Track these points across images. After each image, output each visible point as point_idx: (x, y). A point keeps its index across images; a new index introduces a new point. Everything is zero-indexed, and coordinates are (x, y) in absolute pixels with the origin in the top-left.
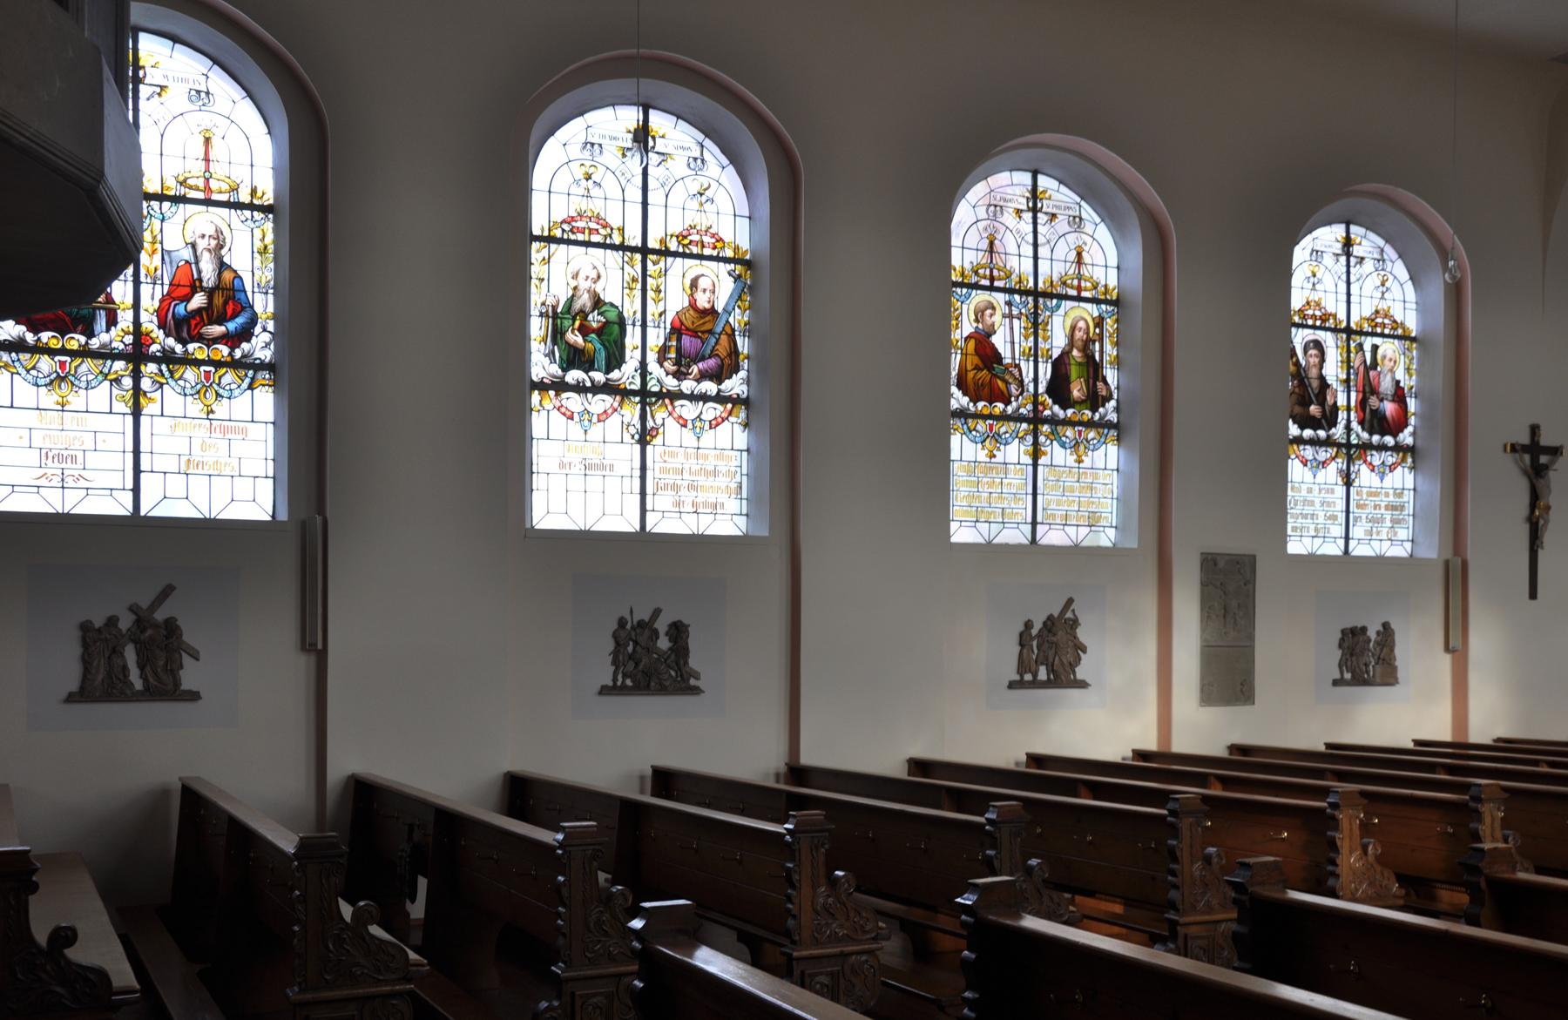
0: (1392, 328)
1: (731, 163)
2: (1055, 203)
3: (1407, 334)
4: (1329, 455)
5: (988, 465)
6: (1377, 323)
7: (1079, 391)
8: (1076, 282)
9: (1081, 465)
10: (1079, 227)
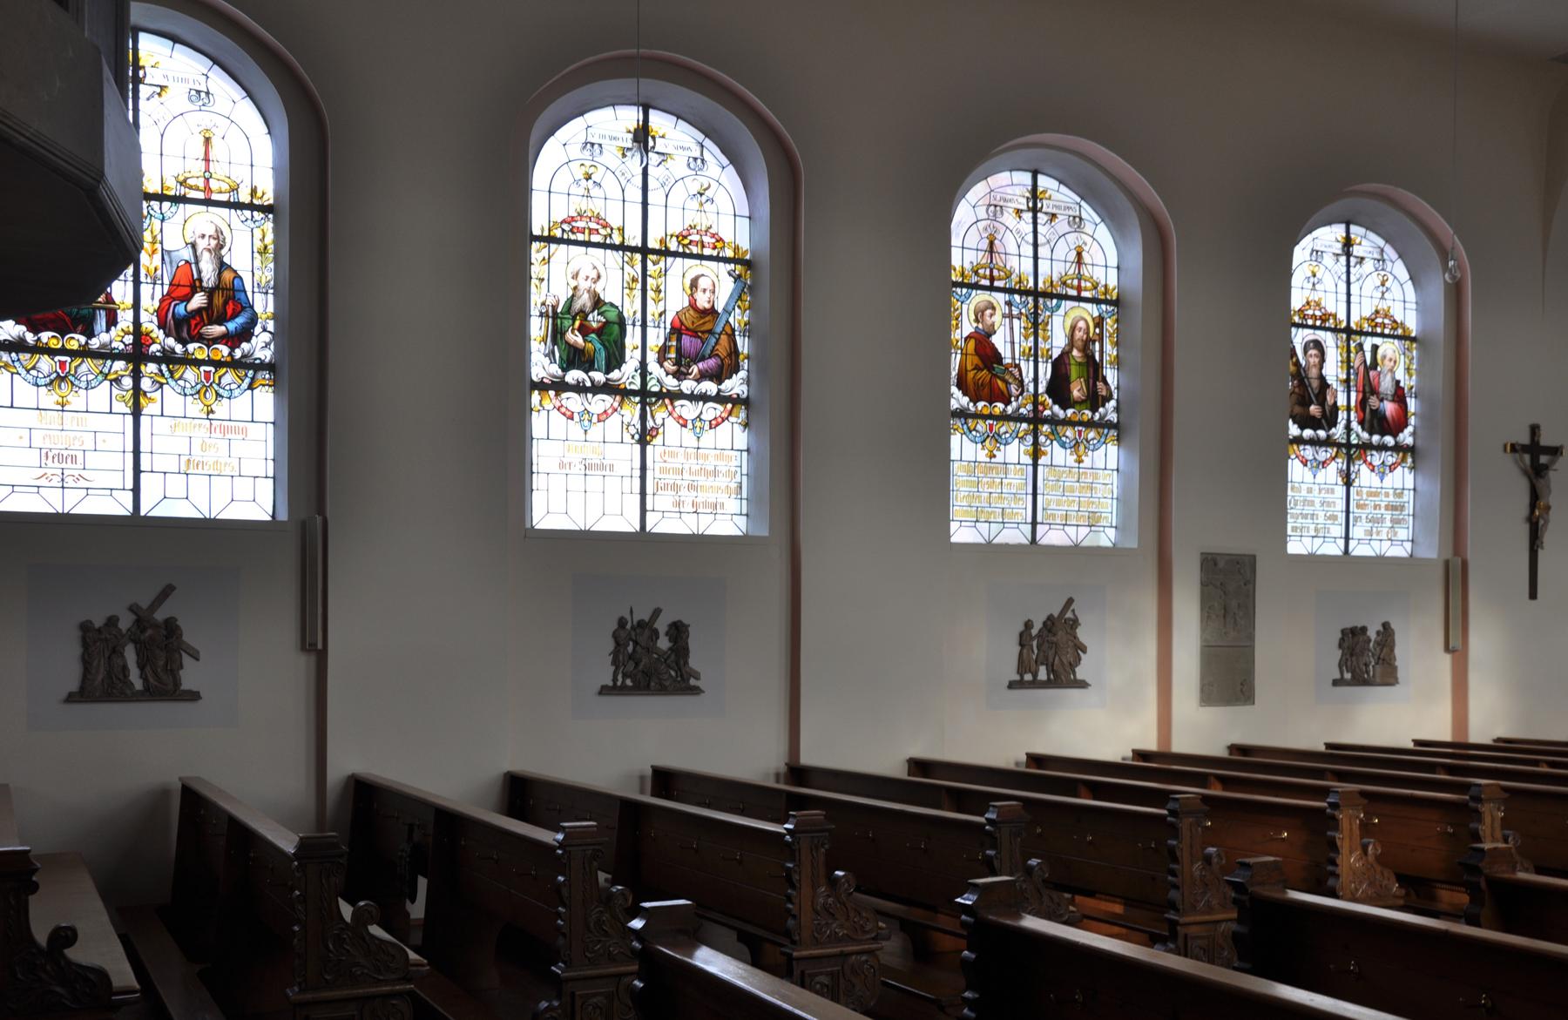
0: (1392, 328)
2: (1055, 203)
3: (1407, 334)
4: (1329, 455)
5: (988, 465)
6: (1377, 323)
7: (1079, 391)
8: (1076, 282)
9: (1081, 465)
10: (1079, 227)
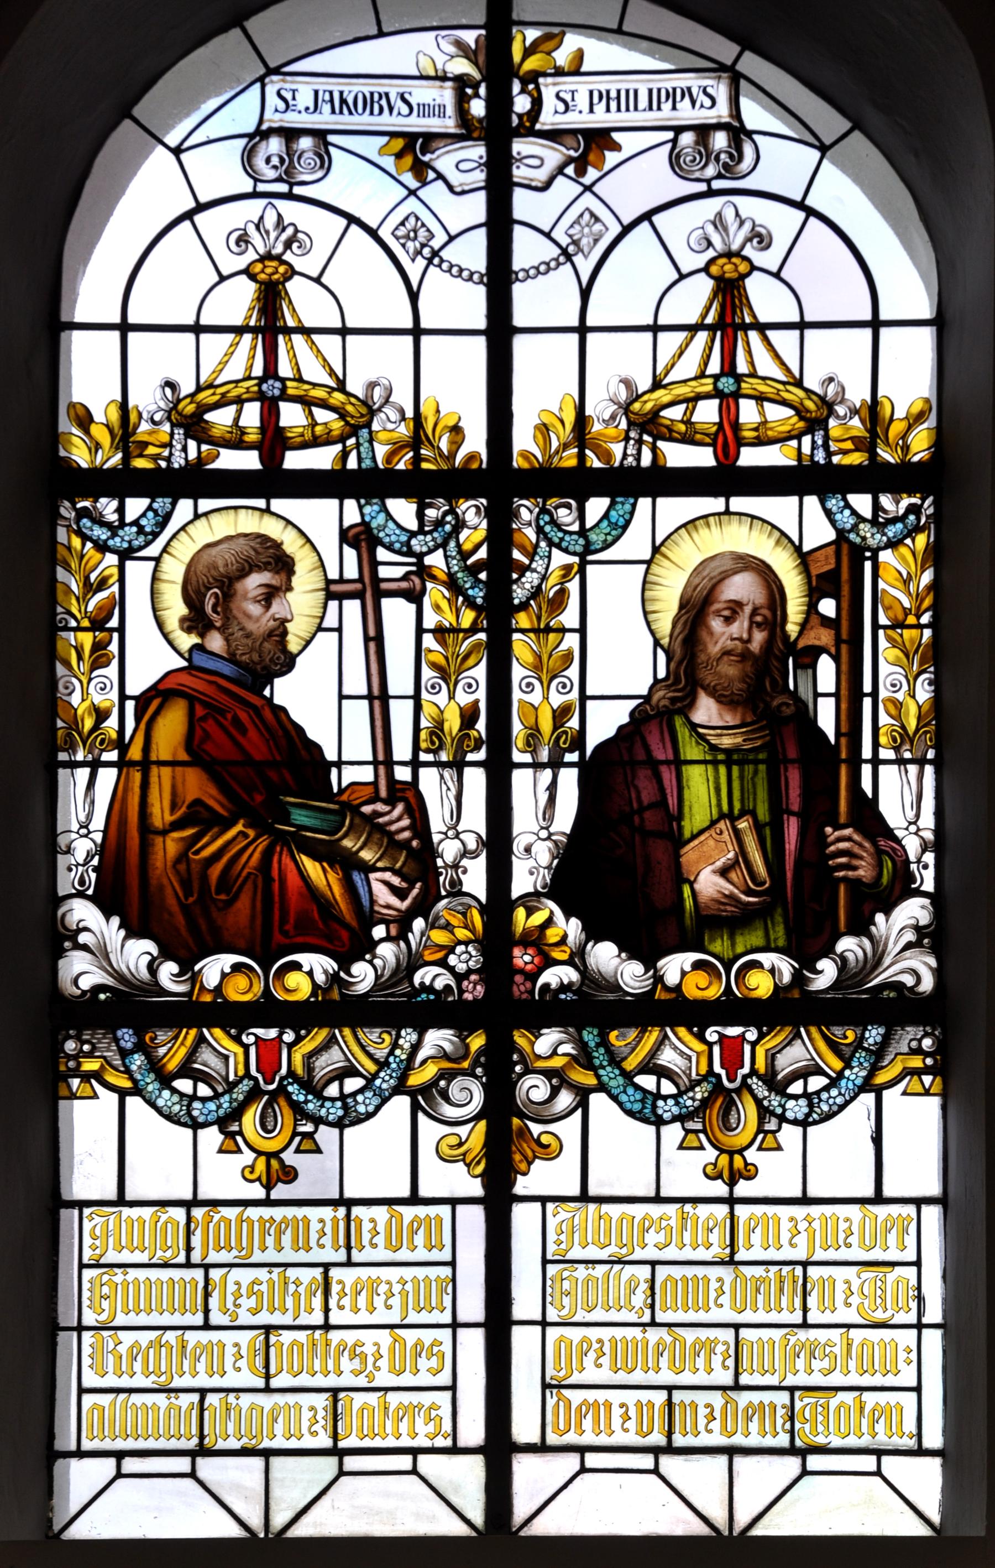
2: (602, 84)
5: (254, 1213)
7: (724, 872)
8: (707, 412)
9: (743, 1189)
10: (728, 171)
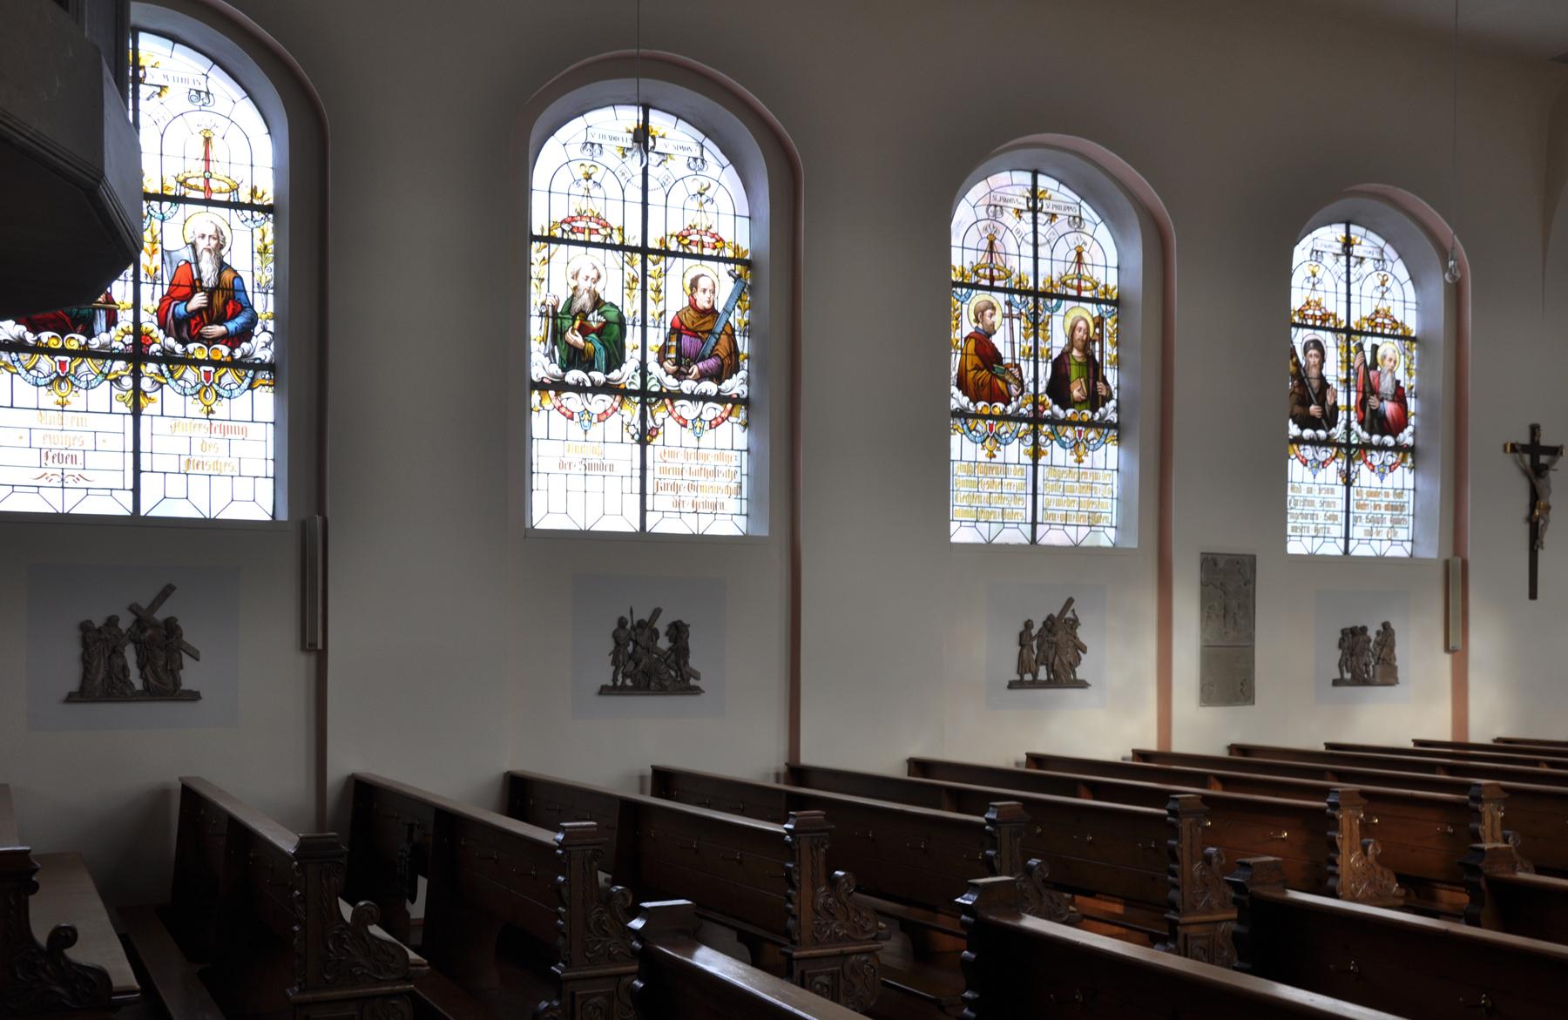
0: (1392, 328)
1: (731, 163)
2: (1055, 203)
3: (1407, 334)
4: (1329, 455)
5: (988, 465)
6: (1377, 323)
7: (1079, 391)
8: (1076, 282)
9: (1081, 465)
10: (1079, 227)
